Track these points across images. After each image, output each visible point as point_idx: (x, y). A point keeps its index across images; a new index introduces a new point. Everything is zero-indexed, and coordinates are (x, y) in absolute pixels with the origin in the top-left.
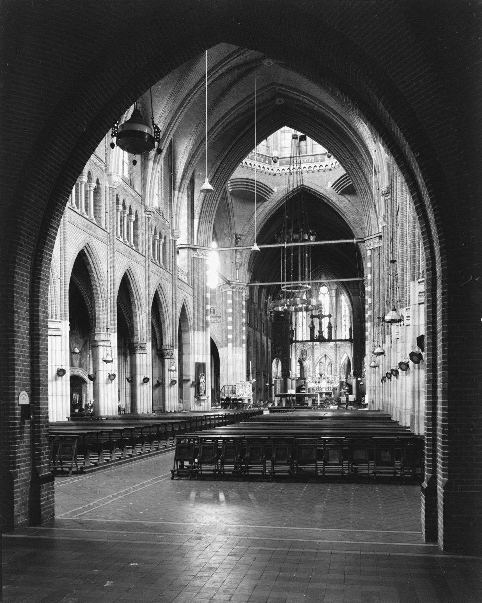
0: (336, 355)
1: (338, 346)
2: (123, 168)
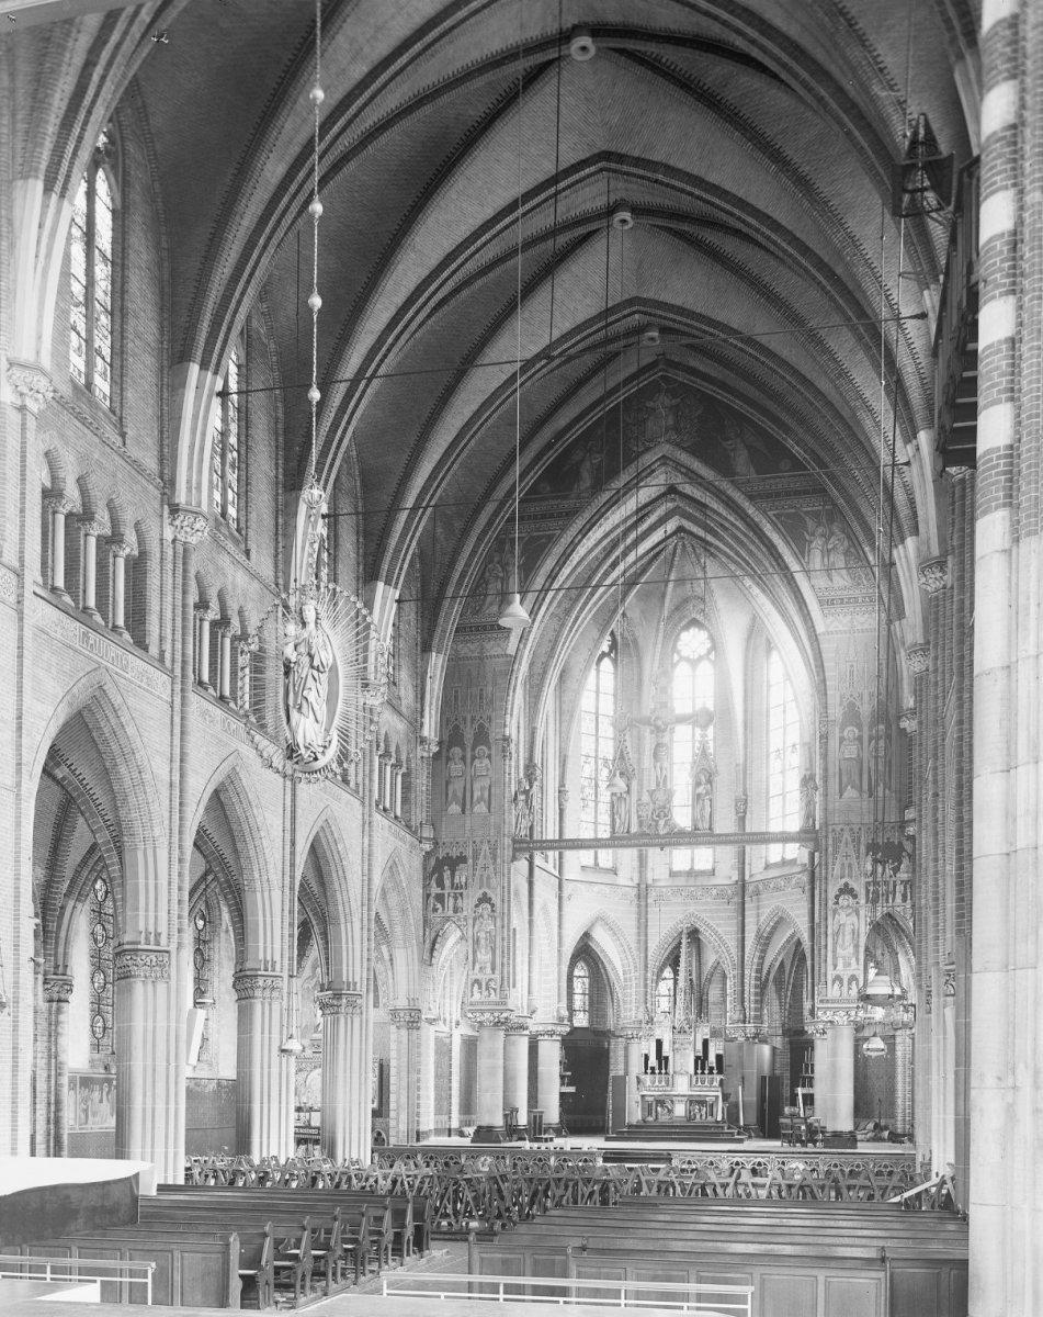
1: (750, 889)
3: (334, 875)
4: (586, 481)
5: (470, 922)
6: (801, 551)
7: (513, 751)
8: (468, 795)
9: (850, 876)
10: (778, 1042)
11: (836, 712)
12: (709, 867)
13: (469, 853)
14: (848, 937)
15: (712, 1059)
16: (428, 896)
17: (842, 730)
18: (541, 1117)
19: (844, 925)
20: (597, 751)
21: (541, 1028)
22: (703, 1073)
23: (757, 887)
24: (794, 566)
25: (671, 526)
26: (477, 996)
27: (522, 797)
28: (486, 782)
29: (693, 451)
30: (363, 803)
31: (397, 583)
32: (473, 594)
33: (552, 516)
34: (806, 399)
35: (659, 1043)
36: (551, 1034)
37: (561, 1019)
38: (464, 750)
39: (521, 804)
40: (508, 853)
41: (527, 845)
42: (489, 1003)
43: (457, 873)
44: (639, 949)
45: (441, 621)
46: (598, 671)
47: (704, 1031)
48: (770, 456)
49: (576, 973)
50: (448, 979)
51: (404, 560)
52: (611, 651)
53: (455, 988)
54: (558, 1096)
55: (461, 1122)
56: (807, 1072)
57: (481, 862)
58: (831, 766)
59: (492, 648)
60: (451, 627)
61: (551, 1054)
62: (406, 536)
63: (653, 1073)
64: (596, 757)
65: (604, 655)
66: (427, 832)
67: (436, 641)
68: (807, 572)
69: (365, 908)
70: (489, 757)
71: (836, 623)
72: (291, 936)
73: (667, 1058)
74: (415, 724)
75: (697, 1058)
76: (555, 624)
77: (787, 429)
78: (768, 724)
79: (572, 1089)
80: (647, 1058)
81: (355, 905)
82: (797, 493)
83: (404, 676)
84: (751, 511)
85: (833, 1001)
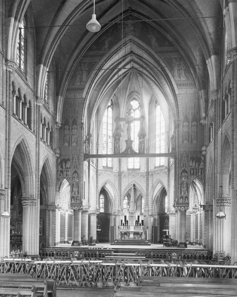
0: (148, 185)
1: (150, 174)
2: (97, 180)
3: (26, 159)
4: (107, 46)
5: (71, 179)
6: (172, 70)
7: (84, 127)
8: (70, 140)
9: (186, 167)
10: (156, 217)
11: (182, 117)
12: (138, 167)
13: (71, 158)
14: (185, 185)
15: (140, 222)
16: (58, 171)
17: (183, 123)
18: (92, 238)
19: (184, 181)
20: (107, 134)
21: (91, 212)
22: (138, 225)
23: (152, 173)
24: (170, 75)
25: (128, 67)
26: (73, 202)
27: (87, 141)
28: (76, 137)
29: (139, 38)
30: (36, 137)
31: (47, 66)
32: (73, 77)
33: (96, 56)
34: (180, 11)
35: (125, 217)
36: (94, 214)
37: (97, 209)
38: (69, 126)
39: (87, 144)
40: (83, 158)
41: (88, 156)
42: (77, 204)
43: (67, 164)
44: (119, 191)
45: (62, 86)
46: (108, 111)
47: (138, 214)
48: (162, 40)
49: (101, 197)
50: (64, 198)
51: (50, 58)
52: (111, 105)
53: (66, 200)
54: (96, 232)
55: (68, 239)
56: (166, 225)
57: (74, 161)
58: (180, 134)
59: (78, 96)
60: (65, 88)
61: (94, 219)
62: (51, 50)
63: (124, 225)
64: (107, 135)
65: (109, 106)
66: (58, 151)
67: (60, 93)
68: (173, 76)
69: (37, 171)
70: (77, 129)
71: (182, 91)
72: (8, 176)
73: (127, 221)
74: (54, 118)
75: (136, 221)
76: (96, 92)
77: (167, 32)
78: (155, 128)
79: (165, 230)
80: (122, 221)
81: (34, 170)
82: (170, 52)
83: (51, 101)
84: (156, 56)
85: (180, 204)
